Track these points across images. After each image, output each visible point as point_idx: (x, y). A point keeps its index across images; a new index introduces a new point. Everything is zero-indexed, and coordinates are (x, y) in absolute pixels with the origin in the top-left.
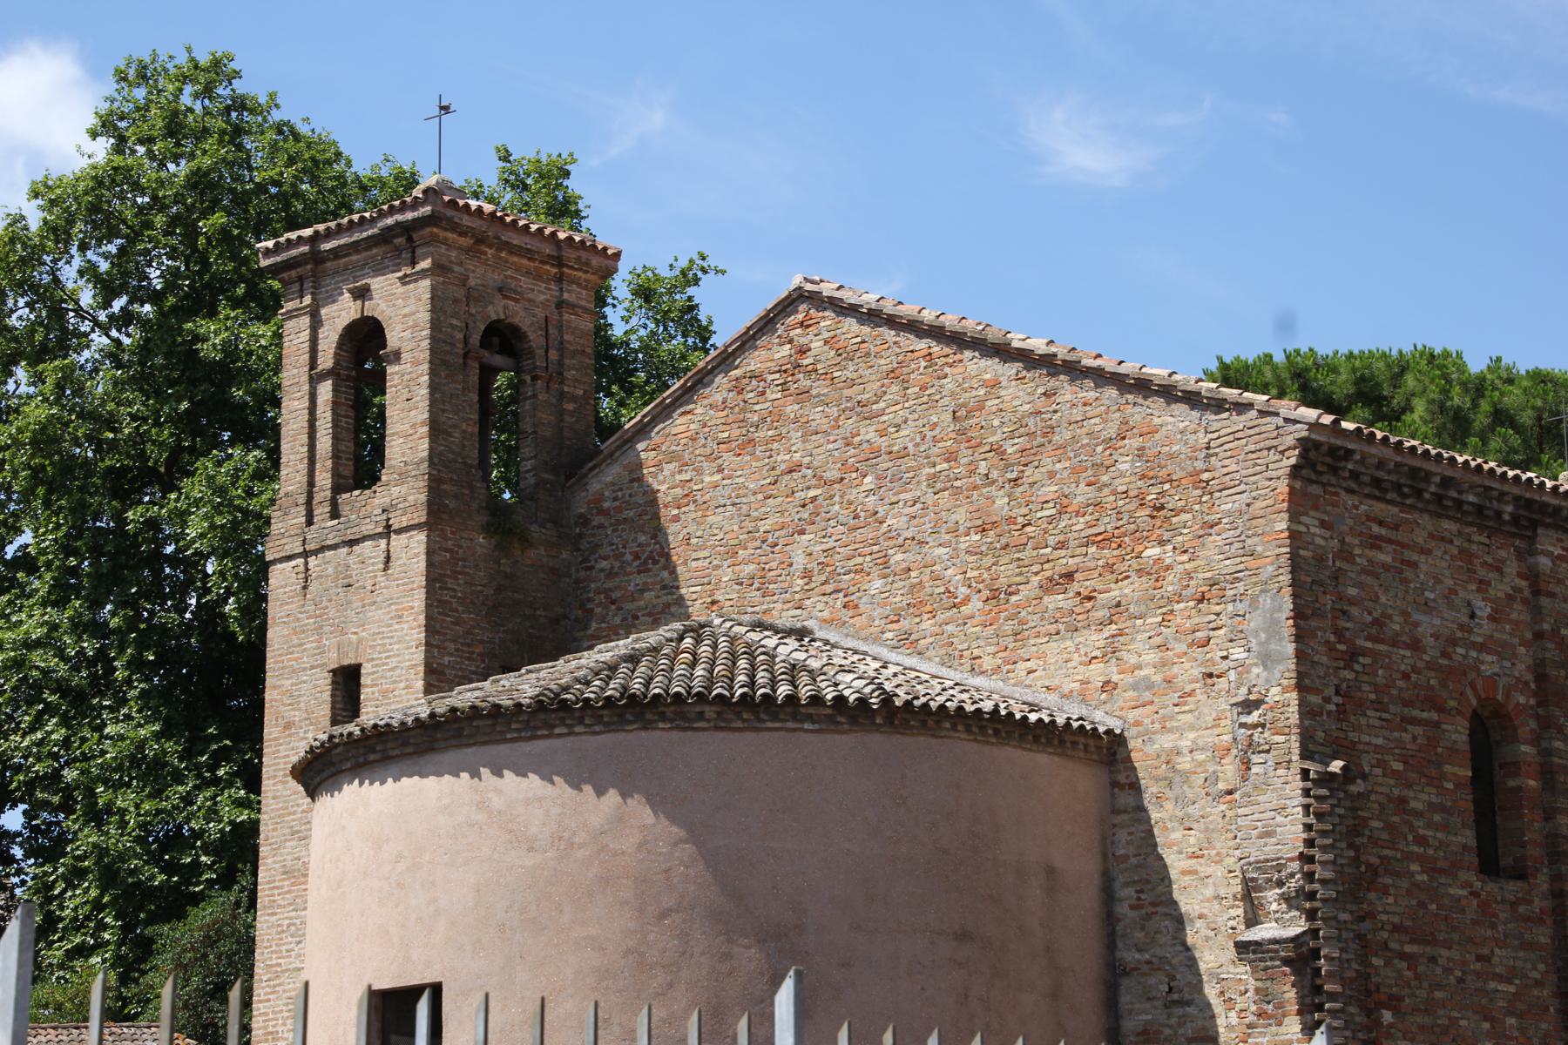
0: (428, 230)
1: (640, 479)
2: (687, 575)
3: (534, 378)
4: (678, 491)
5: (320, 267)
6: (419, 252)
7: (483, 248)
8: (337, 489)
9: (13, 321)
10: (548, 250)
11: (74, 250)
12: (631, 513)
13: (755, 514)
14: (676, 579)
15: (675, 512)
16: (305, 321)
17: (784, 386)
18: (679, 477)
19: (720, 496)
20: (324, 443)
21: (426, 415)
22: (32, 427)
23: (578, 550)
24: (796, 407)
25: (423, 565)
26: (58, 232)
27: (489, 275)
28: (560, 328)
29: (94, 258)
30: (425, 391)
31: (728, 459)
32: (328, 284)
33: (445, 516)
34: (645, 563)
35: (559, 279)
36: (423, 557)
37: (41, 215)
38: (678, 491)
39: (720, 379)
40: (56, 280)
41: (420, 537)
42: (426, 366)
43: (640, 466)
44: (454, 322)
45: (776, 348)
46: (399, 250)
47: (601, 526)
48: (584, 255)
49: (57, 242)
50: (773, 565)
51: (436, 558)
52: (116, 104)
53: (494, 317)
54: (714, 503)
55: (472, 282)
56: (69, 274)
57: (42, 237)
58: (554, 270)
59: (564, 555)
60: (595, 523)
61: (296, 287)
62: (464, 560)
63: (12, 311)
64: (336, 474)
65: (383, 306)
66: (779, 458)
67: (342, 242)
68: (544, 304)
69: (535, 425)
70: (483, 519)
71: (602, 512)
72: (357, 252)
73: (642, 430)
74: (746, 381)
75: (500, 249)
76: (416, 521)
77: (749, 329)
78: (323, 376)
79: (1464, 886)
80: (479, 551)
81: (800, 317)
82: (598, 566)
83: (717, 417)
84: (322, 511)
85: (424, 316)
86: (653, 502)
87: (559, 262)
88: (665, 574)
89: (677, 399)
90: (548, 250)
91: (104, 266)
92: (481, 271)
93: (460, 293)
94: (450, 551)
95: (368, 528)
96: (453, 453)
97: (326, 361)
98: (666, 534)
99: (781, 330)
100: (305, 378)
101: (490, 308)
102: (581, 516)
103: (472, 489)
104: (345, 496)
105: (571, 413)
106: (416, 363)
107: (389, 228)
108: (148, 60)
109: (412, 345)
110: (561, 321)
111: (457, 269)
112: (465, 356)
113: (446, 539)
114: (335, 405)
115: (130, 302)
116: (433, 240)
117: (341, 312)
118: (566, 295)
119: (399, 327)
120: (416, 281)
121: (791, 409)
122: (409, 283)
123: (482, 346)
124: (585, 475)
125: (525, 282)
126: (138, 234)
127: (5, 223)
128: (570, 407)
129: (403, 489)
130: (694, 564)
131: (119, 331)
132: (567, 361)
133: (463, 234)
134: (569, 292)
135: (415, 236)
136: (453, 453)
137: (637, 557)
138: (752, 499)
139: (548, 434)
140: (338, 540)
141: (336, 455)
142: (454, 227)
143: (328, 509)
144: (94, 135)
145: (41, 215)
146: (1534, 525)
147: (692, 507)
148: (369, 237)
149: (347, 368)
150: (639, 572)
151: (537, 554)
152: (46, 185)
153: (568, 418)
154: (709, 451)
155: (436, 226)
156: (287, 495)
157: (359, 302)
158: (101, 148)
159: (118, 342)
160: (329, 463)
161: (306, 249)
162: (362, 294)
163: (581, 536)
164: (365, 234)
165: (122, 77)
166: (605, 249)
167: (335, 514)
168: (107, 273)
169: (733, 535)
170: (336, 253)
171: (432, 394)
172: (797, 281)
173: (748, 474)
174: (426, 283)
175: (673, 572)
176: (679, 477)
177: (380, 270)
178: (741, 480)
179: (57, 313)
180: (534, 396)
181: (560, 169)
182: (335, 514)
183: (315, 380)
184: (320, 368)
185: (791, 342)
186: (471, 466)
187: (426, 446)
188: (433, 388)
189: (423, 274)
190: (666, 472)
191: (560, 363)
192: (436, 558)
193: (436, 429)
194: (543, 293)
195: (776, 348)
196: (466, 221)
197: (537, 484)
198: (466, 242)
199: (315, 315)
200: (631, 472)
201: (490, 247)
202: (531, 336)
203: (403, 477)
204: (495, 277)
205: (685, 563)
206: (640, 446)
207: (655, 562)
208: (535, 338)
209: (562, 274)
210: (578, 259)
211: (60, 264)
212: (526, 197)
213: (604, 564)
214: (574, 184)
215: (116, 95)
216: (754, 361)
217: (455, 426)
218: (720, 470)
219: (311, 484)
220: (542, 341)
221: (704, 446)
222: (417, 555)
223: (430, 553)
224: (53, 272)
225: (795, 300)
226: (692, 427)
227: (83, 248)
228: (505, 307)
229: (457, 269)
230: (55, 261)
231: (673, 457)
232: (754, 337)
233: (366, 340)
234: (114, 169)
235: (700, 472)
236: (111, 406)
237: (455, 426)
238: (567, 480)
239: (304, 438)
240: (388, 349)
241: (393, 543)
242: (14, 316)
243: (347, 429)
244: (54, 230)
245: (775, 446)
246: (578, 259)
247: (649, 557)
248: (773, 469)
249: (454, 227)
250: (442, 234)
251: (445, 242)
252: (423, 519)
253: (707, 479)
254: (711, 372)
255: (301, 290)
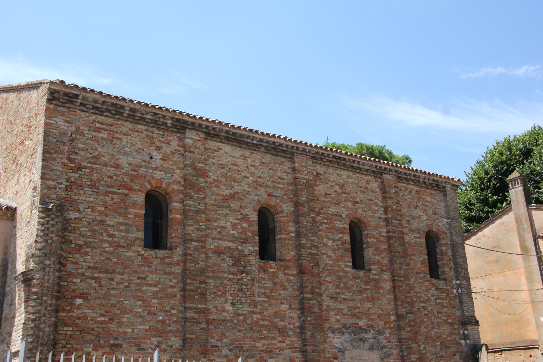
79: (137, 252)
146: (184, 128)
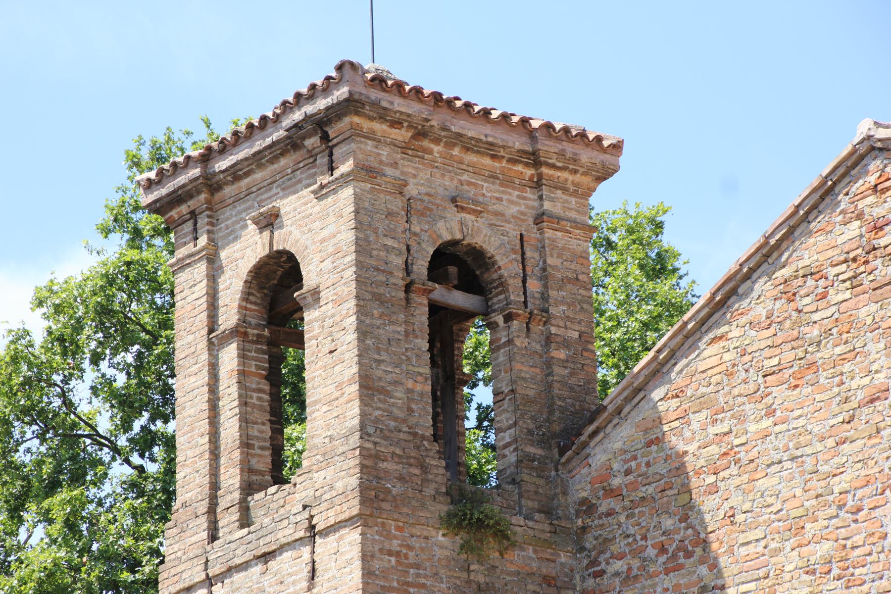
0: (347, 120)
1: (658, 441)
2: (735, 569)
3: (509, 318)
4: (714, 450)
5: (218, 196)
6: (337, 152)
7: (426, 143)
8: (249, 489)
9: (20, 457)
10: (519, 142)
11: (86, 365)
12: (651, 489)
13: (826, 468)
14: (719, 575)
15: (711, 479)
16: (202, 268)
17: (854, 282)
18: (712, 430)
19: (772, 449)
20: (230, 429)
21: (355, 369)
22: (36, 575)
23: (582, 549)
24: (874, 307)
25: (357, 574)
26: (66, 343)
27: (438, 180)
28: (542, 249)
29: (110, 372)
30: (351, 337)
31: (780, 394)
32: (228, 216)
33: (385, 505)
34: (674, 556)
35: (537, 184)
36: (358, 564)
37: (46, 324)
38: (714, 450)
39: (761, 286)
40: (68, 404)
41: (352, 537)
42: (352, 303)
43: (659, 421)
44: (390, 242)
45: (838, 229)
46: (312, 155)
47: (610, 513)
48: (569, 149)
49: (64, 354)
50: (858, 539)
51: (376, 565)
52: (129, 194)
53: (447, 237)
54: (766, 460)
55: (412, 190)
56: (80, 391)
57: (47, 350)
58: (529, 172)
59: (563, 558)
60: (602, 509)
61: (188, 227)
62: (417, 566)
63: (19, 443)
64: (247, 469)
65: (296, 233)
66: (854, 384)
67: (241, 155)
68: (518, 219)
69: (512, 382)
70: (442, 508)
71: (611, 492)
72: (260, 166)
73: (658, 372)
74: (800, 281)
75: (450, 145)
76: (346, 515)
77: (798, 207)
78: (224, 339)
80: (439, 553)
81: (872, 179)
82: (611, 570)
83: (759, 339)
84: (228, 520)
85: (347, 237)
86: (680, 470)
87: (534, 160)
88: (703, 570)
89: (703, 322)
90: (519, 142)
91: (121, 380)
92: (424, 175)
93: (397, 205)
94: (398, 554)
95: (287, 533)
96: (396, 419)
97: (228, 318)
98: (700, 512)
99: (844, 202)
100: (203, 344)
101: (441, 224)
102: (584, 501)
103: (424, 468)
104: (257, 496)
105: (564, 363)
106: (339, 302)
107: (297, 126)
108: (162, 139)
109: (333, 278)
110: (542, 240)
111: (389, 171)
112: (408, 288)
113: (389, 537)
114: (243, 374)
115: (152, 419)
116: (356, 133)
117: (245, 251)
118: (547, 205)
119: (316, 258)
120: (335, 191)
121: (866, 311)
122: (326, 196)
123: (430, 278)
124: (585, 445)
125: (489, 190)
126: (155, 338)
127: (6, 341)
128: (561, 354)
129: (329, 473)
130: (743, 551)
131: (142, 456)
132: (553, 293)
133: (396, 124)
134: (552, 200)
135: (331, 133)
136: (396, 419)
137: (663, 550)
138: (819, 447)
139: (531, 393)
140: (248, 556)
141: (246, 444)
142: (383, 115)
143: (236, 516)
144: (107, 232)
145: (46, 324)
147: (734, 470)
148: (274, 144)
149: (258, 326)
150: (667, 572)
151: (523, 558)
152: (51, 290)
153: (557, 369)
154: (752, 387)
155: (357, 113)
156: (184, 505)
157: (266, 233)
158: (116, 247)
159: (141, 469)
160: (237, 454)
161: (196, 172)
162: (269, 222)
163: (584, 529)
164: (268, 141)
165: (136, 163)
166: (599, 139)
167: (245, 521)
168: (127, 387)
169: (796, 503)
170: (235, 173)
171: (361, 340)
172: (864, 128)
173: (810, 411)
174: (347, 193)
175: (714, 565)
176: (712, 430)
177: (290, 188)
178: (801, 422)
179: (71, 439)
180: (510, 342)
181: (652, 221)
182: (245, 521)
183: (214, 345)
184: (222, 328)
185: (860, 216)
186: (423, 437)
187: (357, 411)
188: (363, 332)
189: (345, 180)
190: (695, 426)
191: (544, 297)
192: (376, 565)
193: (369, 387)
194: (516, 204)
195: (838, 229)
196: (399, 105)
197: (519, 462)
198: (402, 135)
199: (212, 259)
200: (646, 431)
201: (437, 141)
202: (501, 260)
203: (327, 459)
204: (445, 184)
205: (731, 551)
206: (657, 394)
207: (689, 555)
208: (507, 265)
209: (540, 176)
210: (561, 154)
211: (73, 383)
212: (613, 256)
213: (619, 565)
214: (668, 239)
215: (128, 184)
216: (809, 252)
217: (396, 383)
218: (770, 412)
219: (215, 486)
220: (517, 268)
221: (745, 382)
222: (349, 562)
223: (366, 557)
224: (63, 395)
225: (862, 157)
226: (727, 357)
227: (96, 359)
228: (462, 223)
229: (389, 171)
230: (66, 381)
231: (702, 402)
232: (805, 219)
233: (278, 287)
234: (128, 264)
235: (741, 418)
236: (127, 542)
237: (396, 383)
238: (562, 453)
239: (205, 425)
240: (305, 289)
241: (318, 550)
242: (21, 449)
243: (261, 408)
244: (61, 340)
245: (847, 367)
246: (561, 154)
247: (678, 549)
248: (846, 400)
249: (383, 115)
250: (366, 125)
251: (370, 136)
252: (355, 511)
253: (752, 428)
254: (747, 277)
255: (195, 230)
